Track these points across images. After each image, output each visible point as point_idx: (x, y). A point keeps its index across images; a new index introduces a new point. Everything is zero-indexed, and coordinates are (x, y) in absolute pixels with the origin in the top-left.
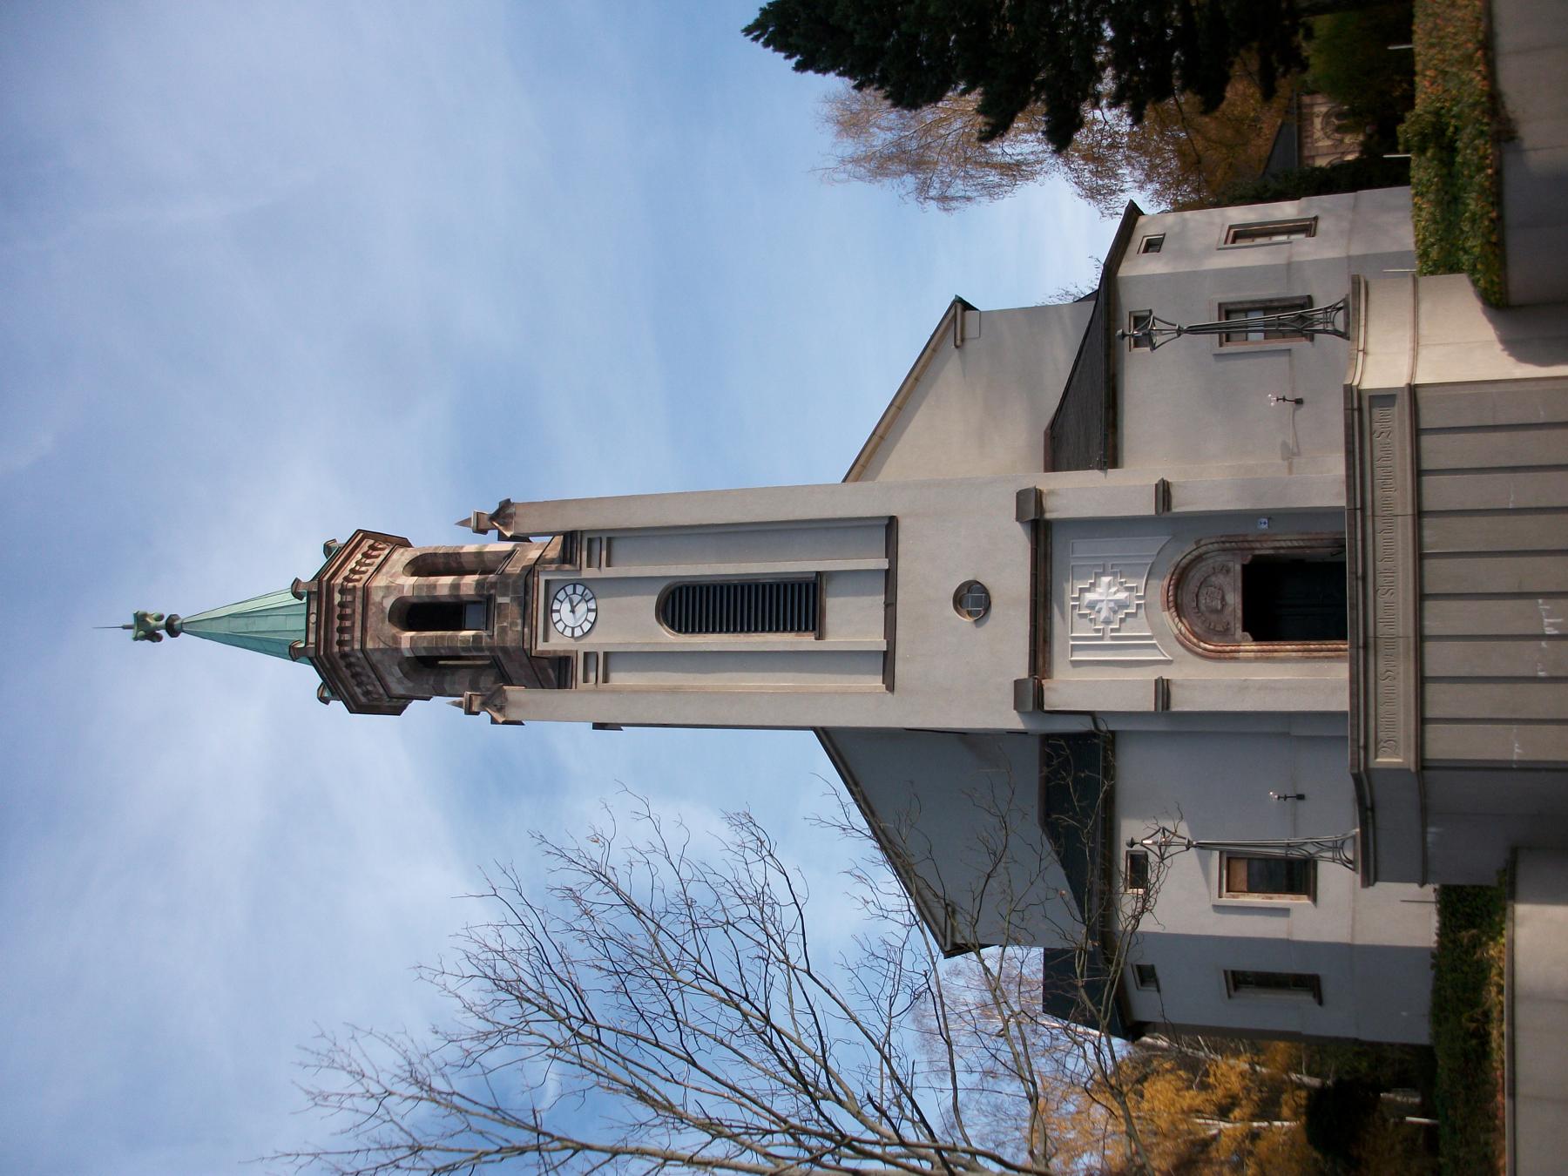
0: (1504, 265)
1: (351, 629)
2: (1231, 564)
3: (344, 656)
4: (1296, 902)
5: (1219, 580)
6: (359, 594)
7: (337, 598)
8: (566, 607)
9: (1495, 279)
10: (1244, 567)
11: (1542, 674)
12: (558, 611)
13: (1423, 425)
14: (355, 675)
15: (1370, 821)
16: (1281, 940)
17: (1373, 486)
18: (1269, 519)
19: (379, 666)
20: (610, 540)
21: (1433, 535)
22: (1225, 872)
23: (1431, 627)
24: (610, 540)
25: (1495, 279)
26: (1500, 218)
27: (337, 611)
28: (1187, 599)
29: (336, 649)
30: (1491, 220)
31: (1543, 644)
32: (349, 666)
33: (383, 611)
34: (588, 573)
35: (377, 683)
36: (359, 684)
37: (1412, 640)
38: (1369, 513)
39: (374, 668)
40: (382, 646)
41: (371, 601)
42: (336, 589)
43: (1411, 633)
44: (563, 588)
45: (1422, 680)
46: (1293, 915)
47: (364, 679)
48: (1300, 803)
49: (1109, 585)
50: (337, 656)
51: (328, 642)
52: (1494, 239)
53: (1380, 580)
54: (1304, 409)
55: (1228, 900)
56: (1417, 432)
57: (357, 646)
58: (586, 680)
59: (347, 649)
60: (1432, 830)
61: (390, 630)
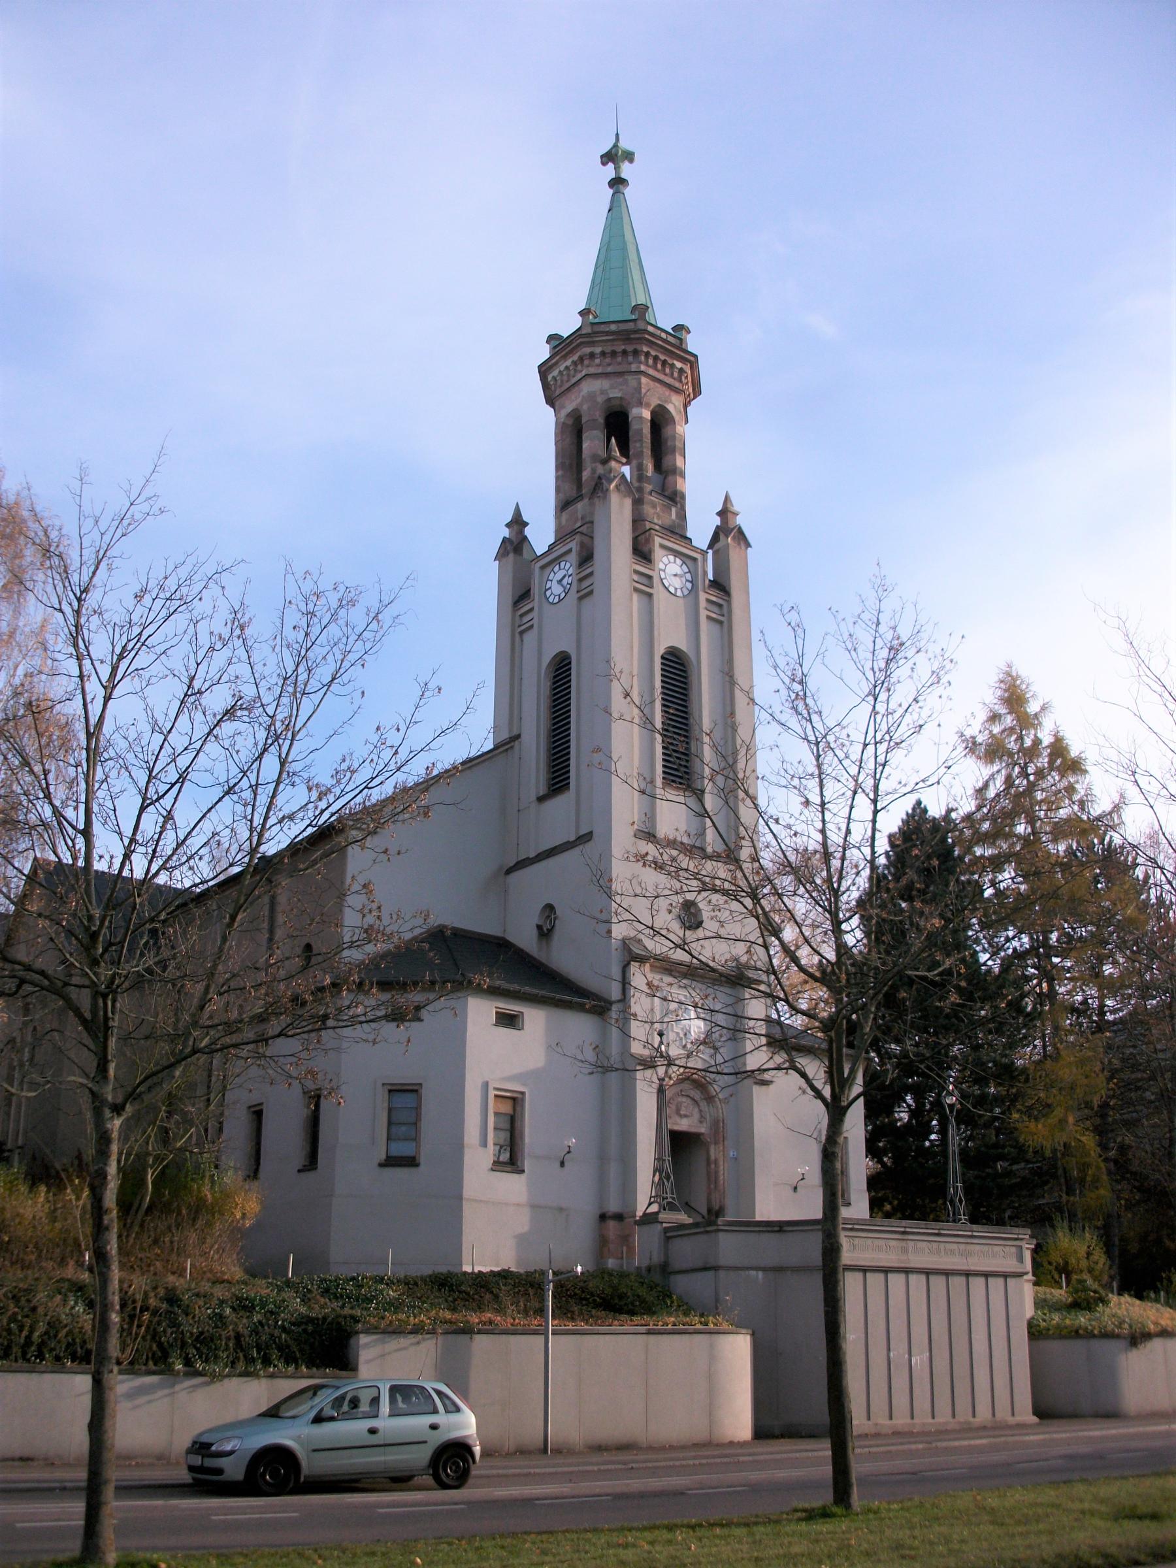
0: (1062, 1337)
1: (655, 367)
2: (705, 1125)
3: (636, 353)
4: (488, 1155)
5: (696, 1116)
6: (677, 384)
7: (679, 365)
8: (678, 570)
9: (1051, 1332)
10: (703, 1134)
11: (892, 1355)
12: (675, 562)
13: (890, 1276)
14: (614, 354)
15: (769, 1229)
16: (462, 1138)
17: (1005, 1245)
18: (736, 1159)
19: (621, 380)
20: (721, 623)
21: (957, 1282)
22: (508, 1094)
23: (913, 1278)
24: (721, 623)
25: (1051, 1332)
26: (1094, 1336)
27: (670, 361)
28: (686, 1086)
29: (645, 349)
30: (1092, 1331)
31: (907, 1356)
32: (624, 352)
33: (666, 401)
34: (703, 597)
35: (600, 370)
36: (603, 354)
37: (907, 1265)
38: (969, 1240)
39: (621, 374)
40: (643, 391)
41: (672, 393)
42: (684, 366)
43: (912, 1265)
44: (690, 572)
45: (886, 1271)
46: (482, 1150)
47: (608, 360)
48: (558, 1164)
49: (699, 1028)
50: (638, 347)
51: (651, 344)
52: (1081, 1332)
53: (935, 1245)
54: (791, 1191)
55: (492, 1093)
56: (1005, 1276)
57: (643, 368)
58: (636, 572)
59: (643, 358)
60: (760, 1274)
61: (654, 402)
